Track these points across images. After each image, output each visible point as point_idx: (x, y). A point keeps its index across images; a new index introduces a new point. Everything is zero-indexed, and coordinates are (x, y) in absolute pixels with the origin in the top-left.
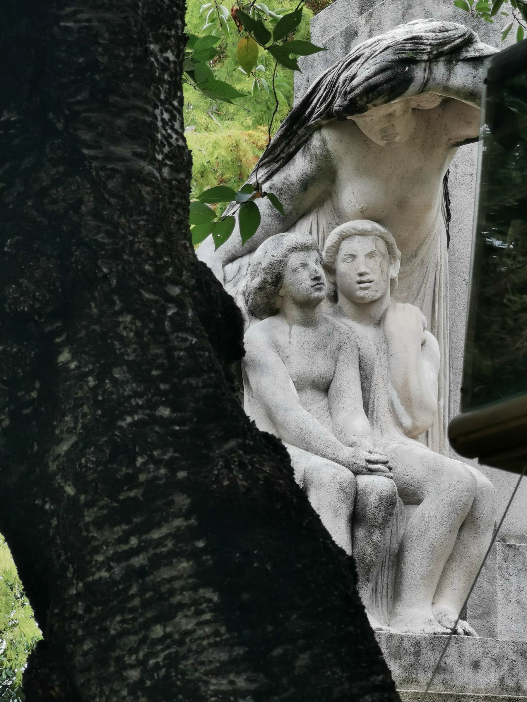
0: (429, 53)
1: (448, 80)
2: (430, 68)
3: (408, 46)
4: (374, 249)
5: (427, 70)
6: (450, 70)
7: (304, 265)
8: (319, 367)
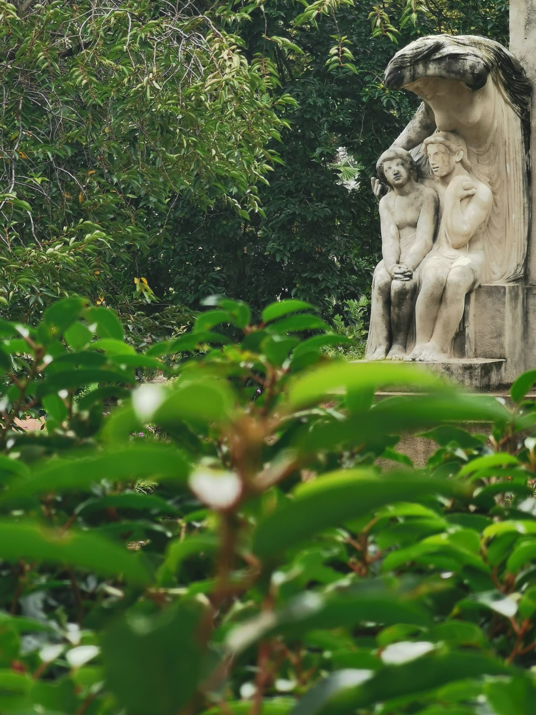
0: (410, 62)
1: (426, 72)
2: (414, 69)
3: (399, 60)
4: (437, 150)
5: (412, 70)
6: (426, 68)
7: (390, 168)
8: (410, 216)
